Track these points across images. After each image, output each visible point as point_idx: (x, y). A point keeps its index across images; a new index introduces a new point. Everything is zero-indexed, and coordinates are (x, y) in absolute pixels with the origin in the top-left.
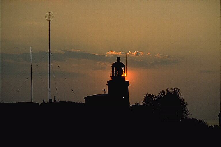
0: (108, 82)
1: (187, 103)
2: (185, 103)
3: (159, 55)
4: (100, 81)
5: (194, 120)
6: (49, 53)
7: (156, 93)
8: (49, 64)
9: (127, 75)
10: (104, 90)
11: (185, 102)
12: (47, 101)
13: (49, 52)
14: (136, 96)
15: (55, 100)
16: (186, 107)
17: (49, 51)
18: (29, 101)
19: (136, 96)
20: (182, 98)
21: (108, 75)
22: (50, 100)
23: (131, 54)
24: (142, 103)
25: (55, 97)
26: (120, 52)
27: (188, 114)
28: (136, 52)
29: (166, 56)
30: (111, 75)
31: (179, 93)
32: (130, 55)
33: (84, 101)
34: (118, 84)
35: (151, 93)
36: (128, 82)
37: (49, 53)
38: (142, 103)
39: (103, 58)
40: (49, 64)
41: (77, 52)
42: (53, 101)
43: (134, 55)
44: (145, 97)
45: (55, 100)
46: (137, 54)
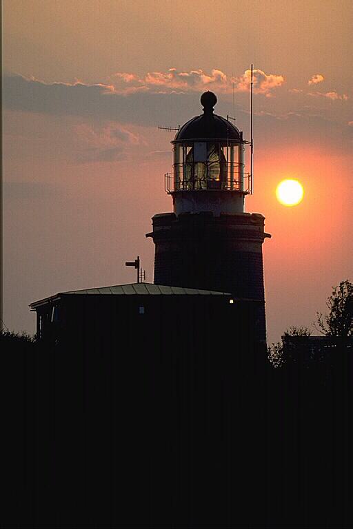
0: (159, 220)
10: (137, 264)
14: (293, 305)
19: (293, 305)
21: (153, 187)
34: (210, 236)
36: (258, 220)
44: (336, 301)
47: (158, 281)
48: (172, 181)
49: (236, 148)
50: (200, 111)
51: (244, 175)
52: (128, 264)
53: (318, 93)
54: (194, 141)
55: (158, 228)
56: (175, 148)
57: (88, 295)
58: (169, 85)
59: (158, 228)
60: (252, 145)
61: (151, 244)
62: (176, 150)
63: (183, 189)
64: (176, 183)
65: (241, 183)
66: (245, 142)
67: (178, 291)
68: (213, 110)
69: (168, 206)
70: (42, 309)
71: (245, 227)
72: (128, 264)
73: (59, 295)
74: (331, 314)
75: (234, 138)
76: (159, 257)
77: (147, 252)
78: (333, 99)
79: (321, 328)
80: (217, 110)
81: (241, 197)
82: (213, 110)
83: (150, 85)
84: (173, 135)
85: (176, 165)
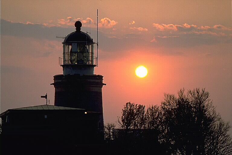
0: (56, 78)
10: (46, 97)
16: (228, 133)
21: (53, 62)
34: (79, 83)
35: (137, 102)
36: (100, 77)
47: (56, 103)
48: (63, 60)
49: (90, 46)
50: (74, 30)
51: (94, 58)
52: (42, 97)
53: (134, 27)
54: (72, 43)
55: (57, 81)
56: (64, 45)
57: (22, 110)
58: (68, 24)
59: (57, 81)
60: (98, 45)
61: (53, 89)
62: (64, 47)
63: (67, 63)
64: (64, 61)
65: (92, 61)
66: (94, 43)
67: (62, 108)
69: (60, 71)
71: (94, 80)
72: (42, 97)
73: (9, 110)
74: (122, 117)
76: (56, 93)
77: (51, 92)
78: (141, 30)
79: (119, 123)
80: (82, 30)
81: (92, 67)
83: (60, 24)
84: (63, 40)
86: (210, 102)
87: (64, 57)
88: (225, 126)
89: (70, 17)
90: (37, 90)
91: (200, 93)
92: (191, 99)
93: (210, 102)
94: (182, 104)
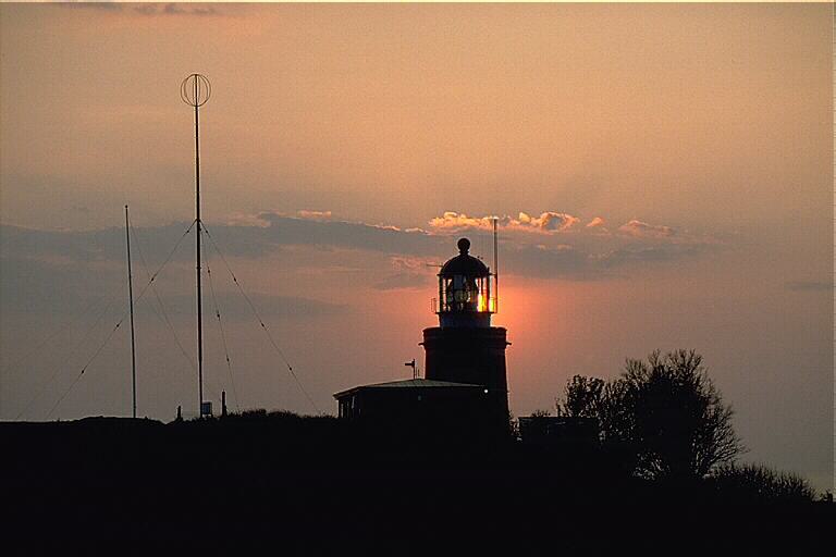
0: (428, 332)
1: (732, 409)
2: (726, 406)
3: (637, 225)
4: (392, 338)
5: (753, 481)
6: (199, 229)
7: (610, 371)
8: (199, 268)
9: (500, 304)
10: (413, 364)
11: (725, 403)
12: (192, 412)
13: (198, 225)
14: (533, 389)
15: (224, 408)
16: (729, 422)
17: (198, 220)
18: (123, 412)
19: (533, 389)
20: (712, 388)
21: (426, 308)
22: (206, 407)
23: (528, 224)
24: (559, 410)
25: (224, 393)
26: (486, 218)
27: (736, 451)
28: (545, 214)
29: (662, 230)
30: (438, 305)
31: (701, 368)
32: (520, 227)
33: (333, 410)
34: (466, 344)
35: (590, 375)
36: (502, 331)
37: (199, 229)
38: (559, 410)
39: (416, 243)
40: (199, 268)
41: (318, 221)
42: (217, 411)
43: (538, 230)
44: (571, 389)
45: (224, 408)
46: (552, 222)
48: (438, 303)
62: (441, 281)
68: (487, 314)
70: (343, 398)
75: (484, 273)
77: (421, 356)
82: (487, 314)
85: (441, 292)
86: (703, 371)
87: (441, 298)
88: (724, 412)
89: (496, 218)
90: (399, 358)
91: (687, 358)
92: (668, 364)
93: (703, 371)
94: (659, 375)
